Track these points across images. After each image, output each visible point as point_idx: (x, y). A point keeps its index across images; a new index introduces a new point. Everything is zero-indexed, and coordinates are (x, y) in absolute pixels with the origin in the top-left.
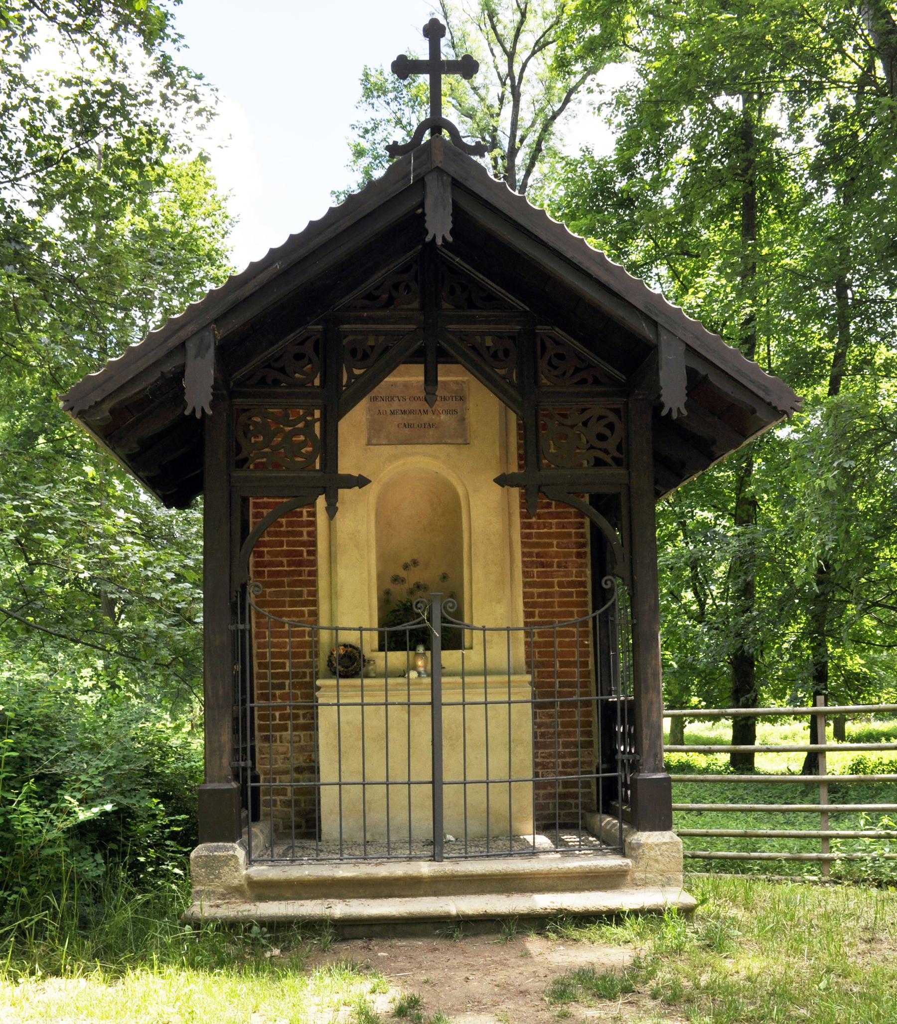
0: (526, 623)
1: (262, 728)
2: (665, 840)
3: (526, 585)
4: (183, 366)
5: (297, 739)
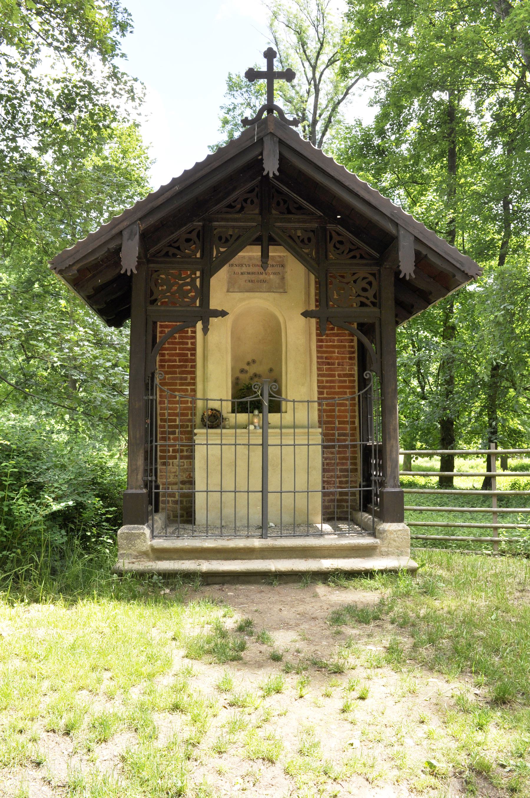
0: (319, 398)
1: (162, 457)
3: (319, 375)
5: (182, 464)
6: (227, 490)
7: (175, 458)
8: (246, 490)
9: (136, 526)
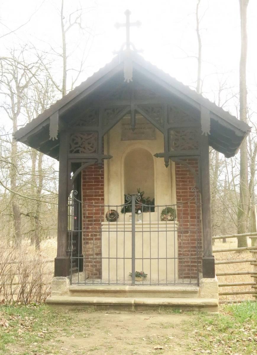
0: (177, 203)
1: (84, 239)
2: (212, 281)
3: (177, 189)
4: (49, 124)
5: (96, 243)
6: (104, 257)
7: (92, 239)
8: (143, 259)
9: (61, 277)
